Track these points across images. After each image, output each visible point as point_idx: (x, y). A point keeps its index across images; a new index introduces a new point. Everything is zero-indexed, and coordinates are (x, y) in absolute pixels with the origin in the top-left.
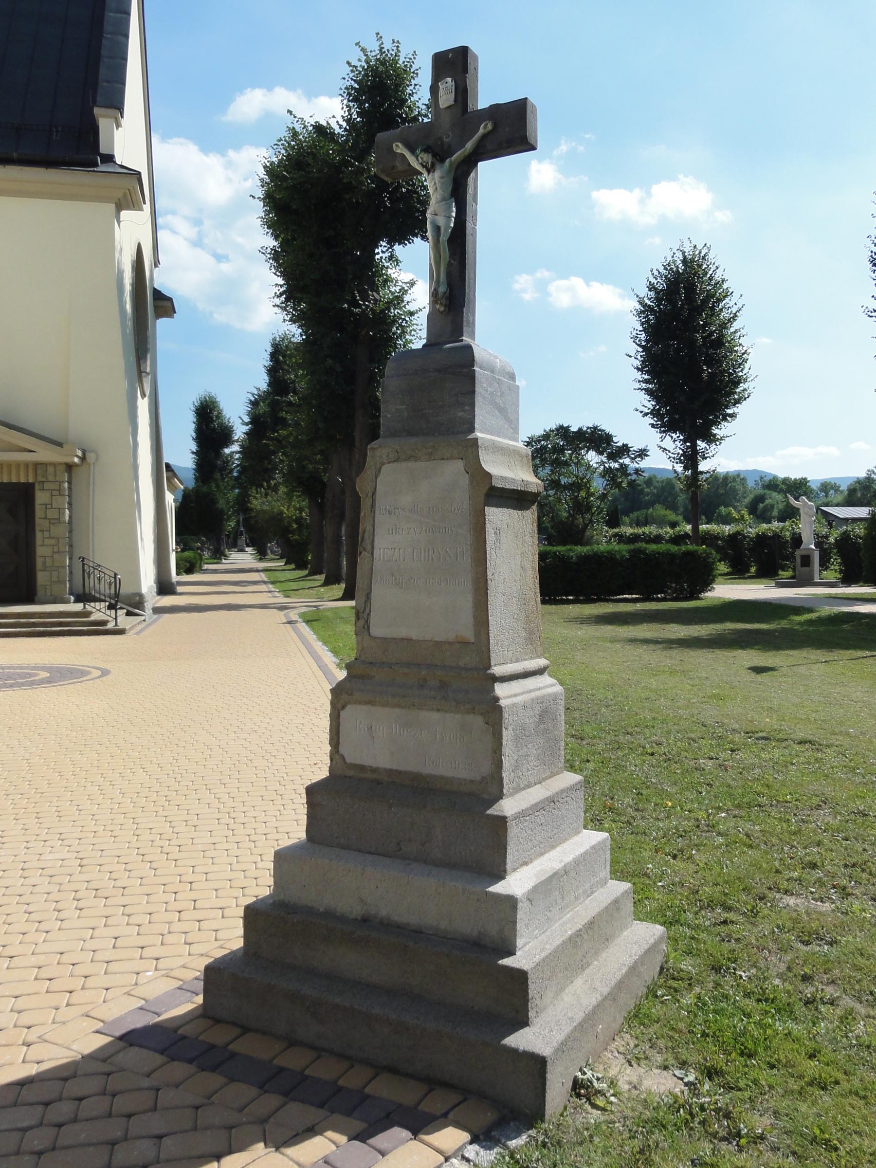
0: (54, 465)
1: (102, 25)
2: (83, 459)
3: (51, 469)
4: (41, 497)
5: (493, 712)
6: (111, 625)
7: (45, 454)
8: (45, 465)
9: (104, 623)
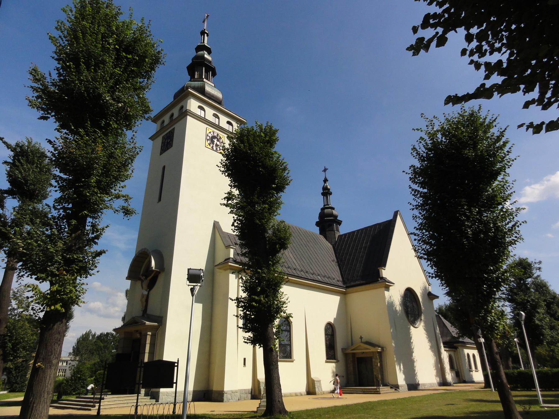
4: (374, 360)
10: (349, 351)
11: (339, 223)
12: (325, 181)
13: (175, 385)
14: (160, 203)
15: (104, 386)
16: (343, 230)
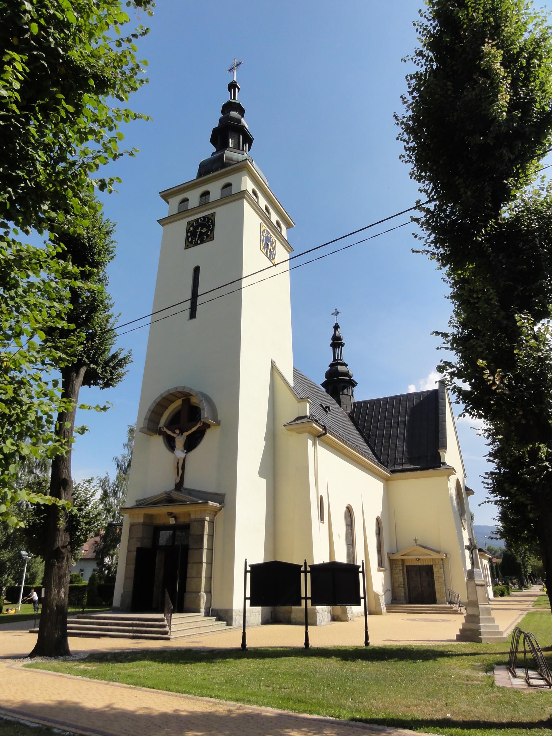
0: (438, 559)
1: (438, 444)
2: (446, 556)
3: (437, 560)
4: (435, 570)
5: (478, 607)
6: (459, 612)
7: (435, 556)
8: (435, 559)
9: (457, 611)
10: (398, 557)
11: (353, 384)
12: (336, 327)
13: (362, 601)
14: (193, 320)
15: (248, 602)
16: (360, 394)
